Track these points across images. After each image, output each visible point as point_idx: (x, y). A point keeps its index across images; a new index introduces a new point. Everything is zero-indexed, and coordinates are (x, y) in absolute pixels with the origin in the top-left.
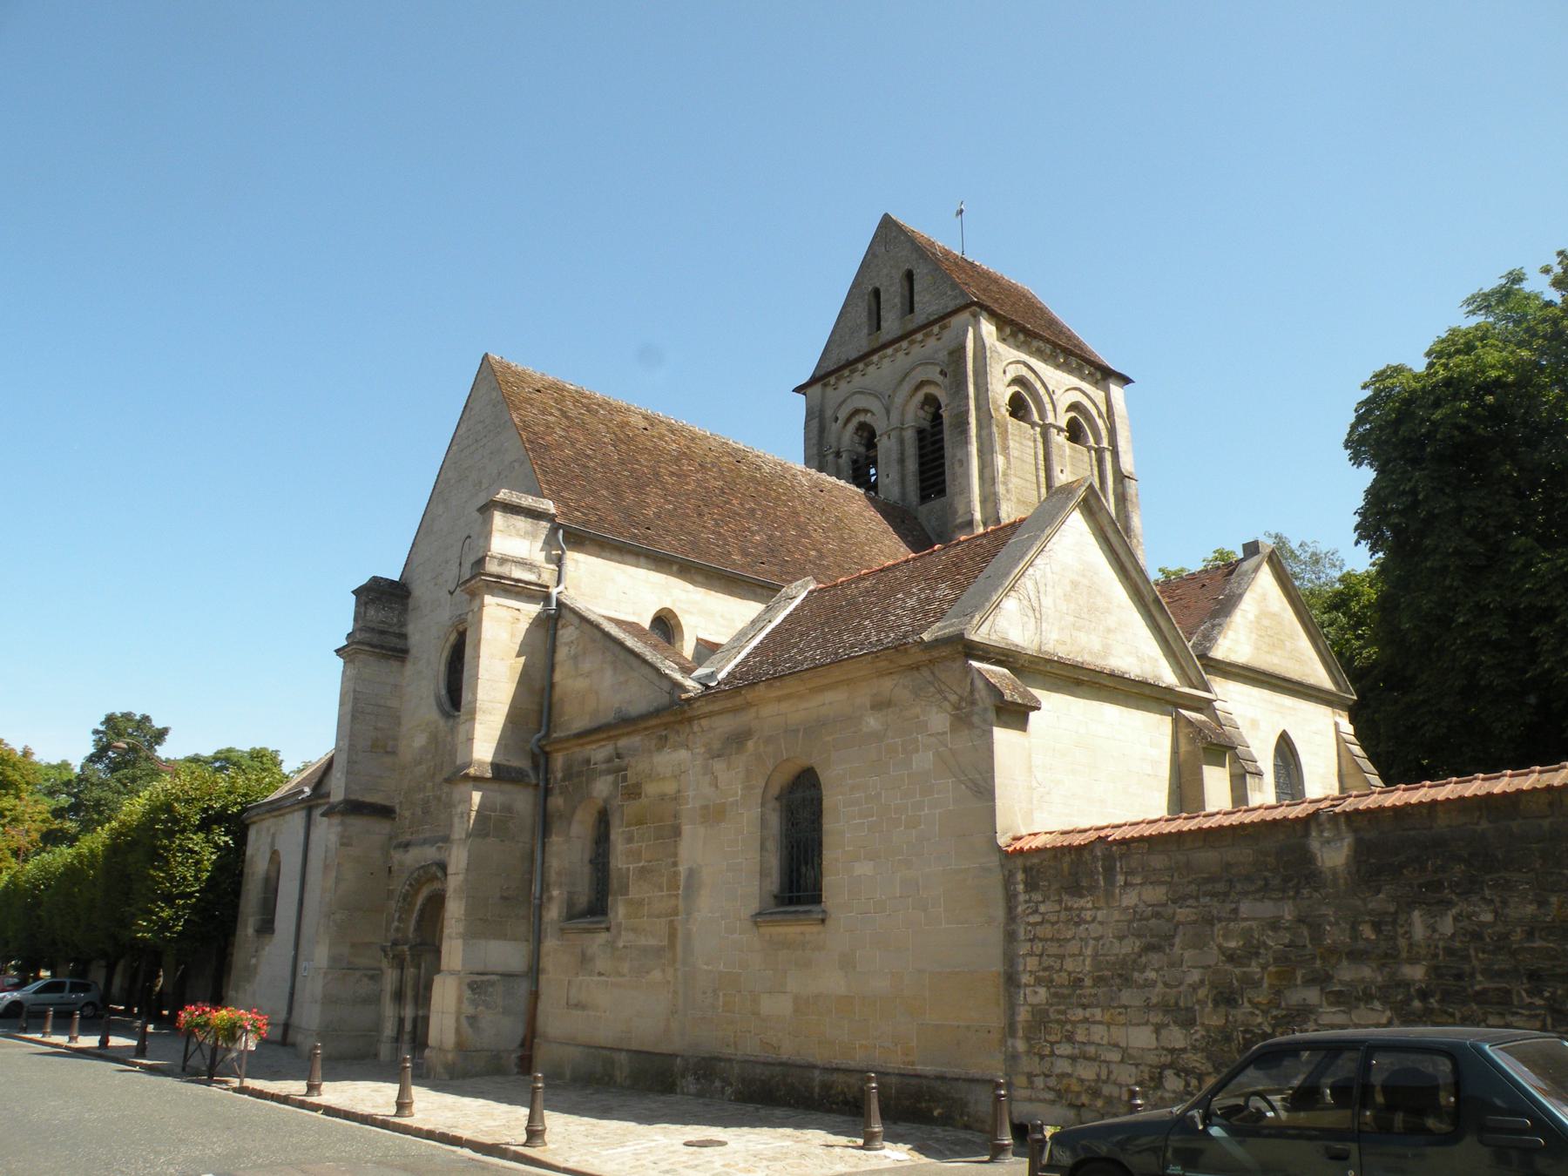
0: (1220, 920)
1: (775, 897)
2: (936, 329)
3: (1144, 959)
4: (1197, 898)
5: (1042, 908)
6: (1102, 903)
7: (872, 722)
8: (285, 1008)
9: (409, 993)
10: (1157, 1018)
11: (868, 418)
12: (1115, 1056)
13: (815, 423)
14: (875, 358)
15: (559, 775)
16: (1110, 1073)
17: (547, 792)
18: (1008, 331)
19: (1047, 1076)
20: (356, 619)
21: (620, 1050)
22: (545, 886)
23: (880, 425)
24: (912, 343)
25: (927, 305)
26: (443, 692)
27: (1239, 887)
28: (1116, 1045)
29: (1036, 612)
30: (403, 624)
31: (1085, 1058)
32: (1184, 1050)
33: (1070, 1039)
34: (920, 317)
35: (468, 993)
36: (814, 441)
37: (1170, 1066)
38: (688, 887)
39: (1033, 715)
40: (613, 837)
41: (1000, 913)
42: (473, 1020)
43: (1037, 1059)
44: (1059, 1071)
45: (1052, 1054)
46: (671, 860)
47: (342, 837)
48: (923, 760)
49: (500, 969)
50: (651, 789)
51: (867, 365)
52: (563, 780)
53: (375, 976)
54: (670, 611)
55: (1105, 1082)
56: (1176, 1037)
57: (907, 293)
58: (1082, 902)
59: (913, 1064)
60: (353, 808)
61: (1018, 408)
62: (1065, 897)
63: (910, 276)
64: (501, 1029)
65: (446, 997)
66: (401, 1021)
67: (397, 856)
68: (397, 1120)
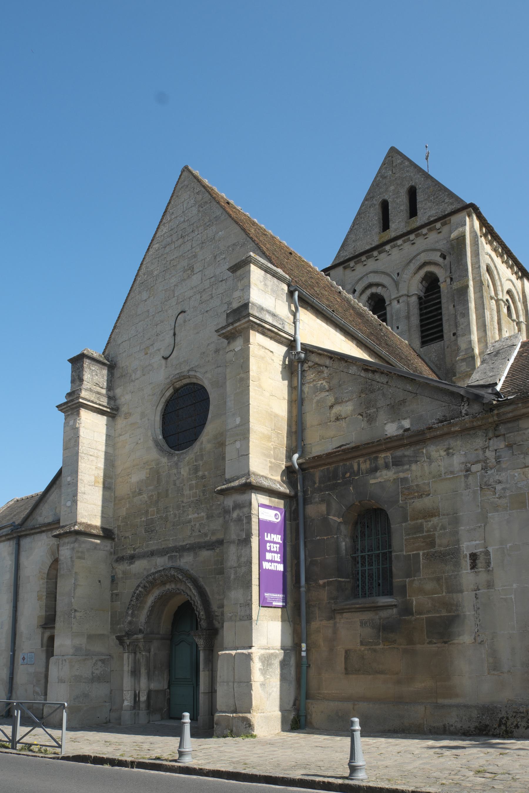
9: (143, 671)
11: (379, 290)
25: (427, 211)
26: (161, 437)
34: (422, 218)
63: (412, 193)
66: (136, 696)
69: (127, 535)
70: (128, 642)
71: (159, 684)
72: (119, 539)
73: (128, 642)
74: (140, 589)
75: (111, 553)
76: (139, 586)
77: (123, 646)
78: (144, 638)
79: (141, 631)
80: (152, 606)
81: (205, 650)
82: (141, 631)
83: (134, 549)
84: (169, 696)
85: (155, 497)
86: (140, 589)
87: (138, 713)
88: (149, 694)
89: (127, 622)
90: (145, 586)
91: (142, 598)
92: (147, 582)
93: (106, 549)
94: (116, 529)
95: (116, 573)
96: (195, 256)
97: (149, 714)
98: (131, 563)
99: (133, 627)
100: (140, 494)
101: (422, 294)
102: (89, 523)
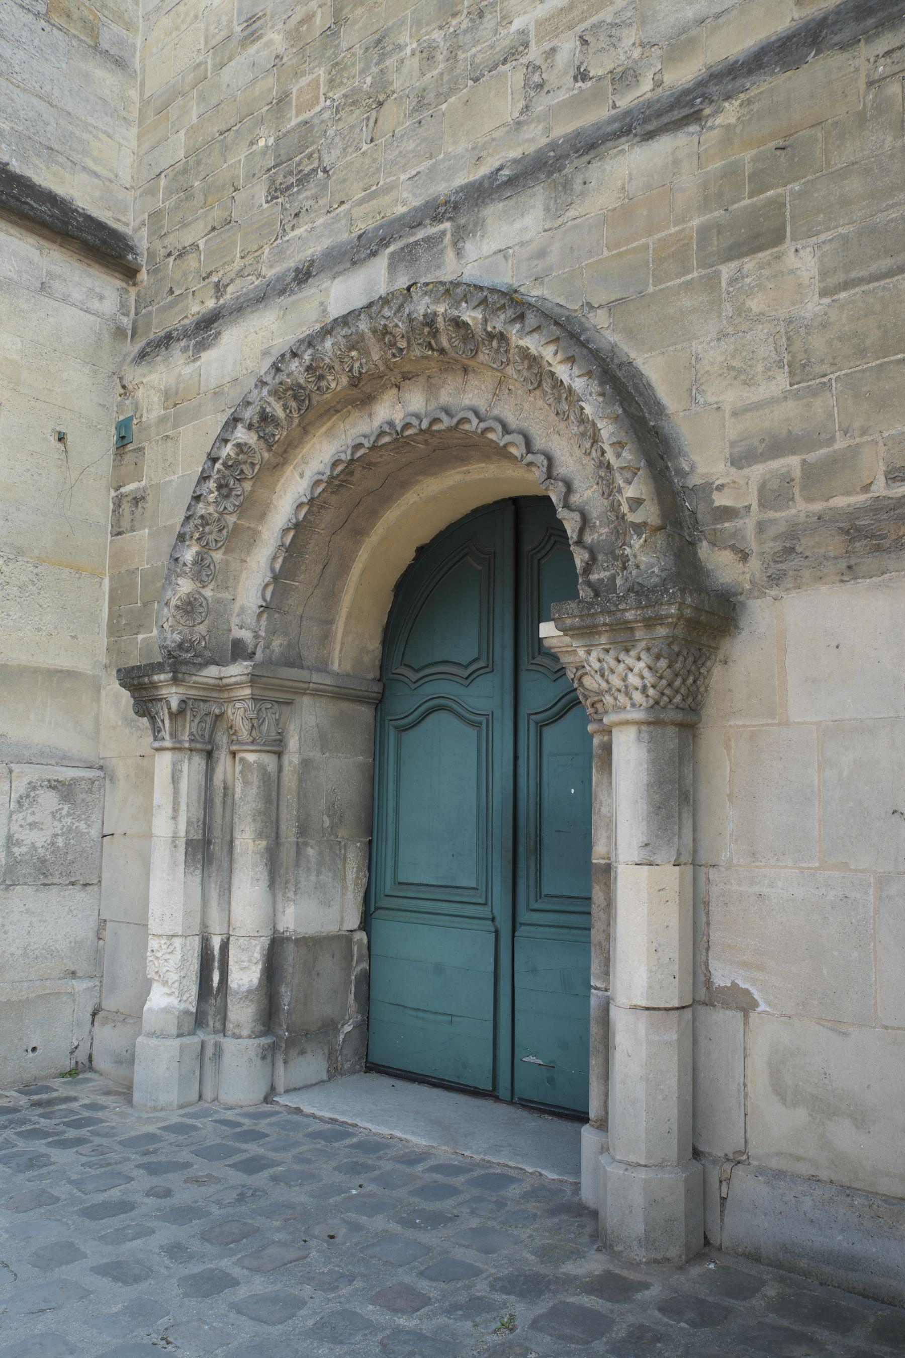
66: (210, 964)
69: (187, 238)
70: (173, 695)
71: (324, 908)
72: (152, 272)
73: (173, 695)
74: (241, 434)
75: (119, 333)
76: (235, 420)
77: (153, 720)
78: (254, 679)
79: (238, 651)
80: (297, 526)
81: (656, 723)
82: (238, 651)
83: (219, 289)
84: (365, 965)
86: (241, 434)
87: (218, 1052)
89: (173, 602)
90: (265, 418)
91: (248, 486)
92: (274, 393)
93: (95, 305)
94: (145, 232)
95: (137, 407)
97: (269, 1054)
98: (202, 346)
99: (202, 629)
100: (251, 36)
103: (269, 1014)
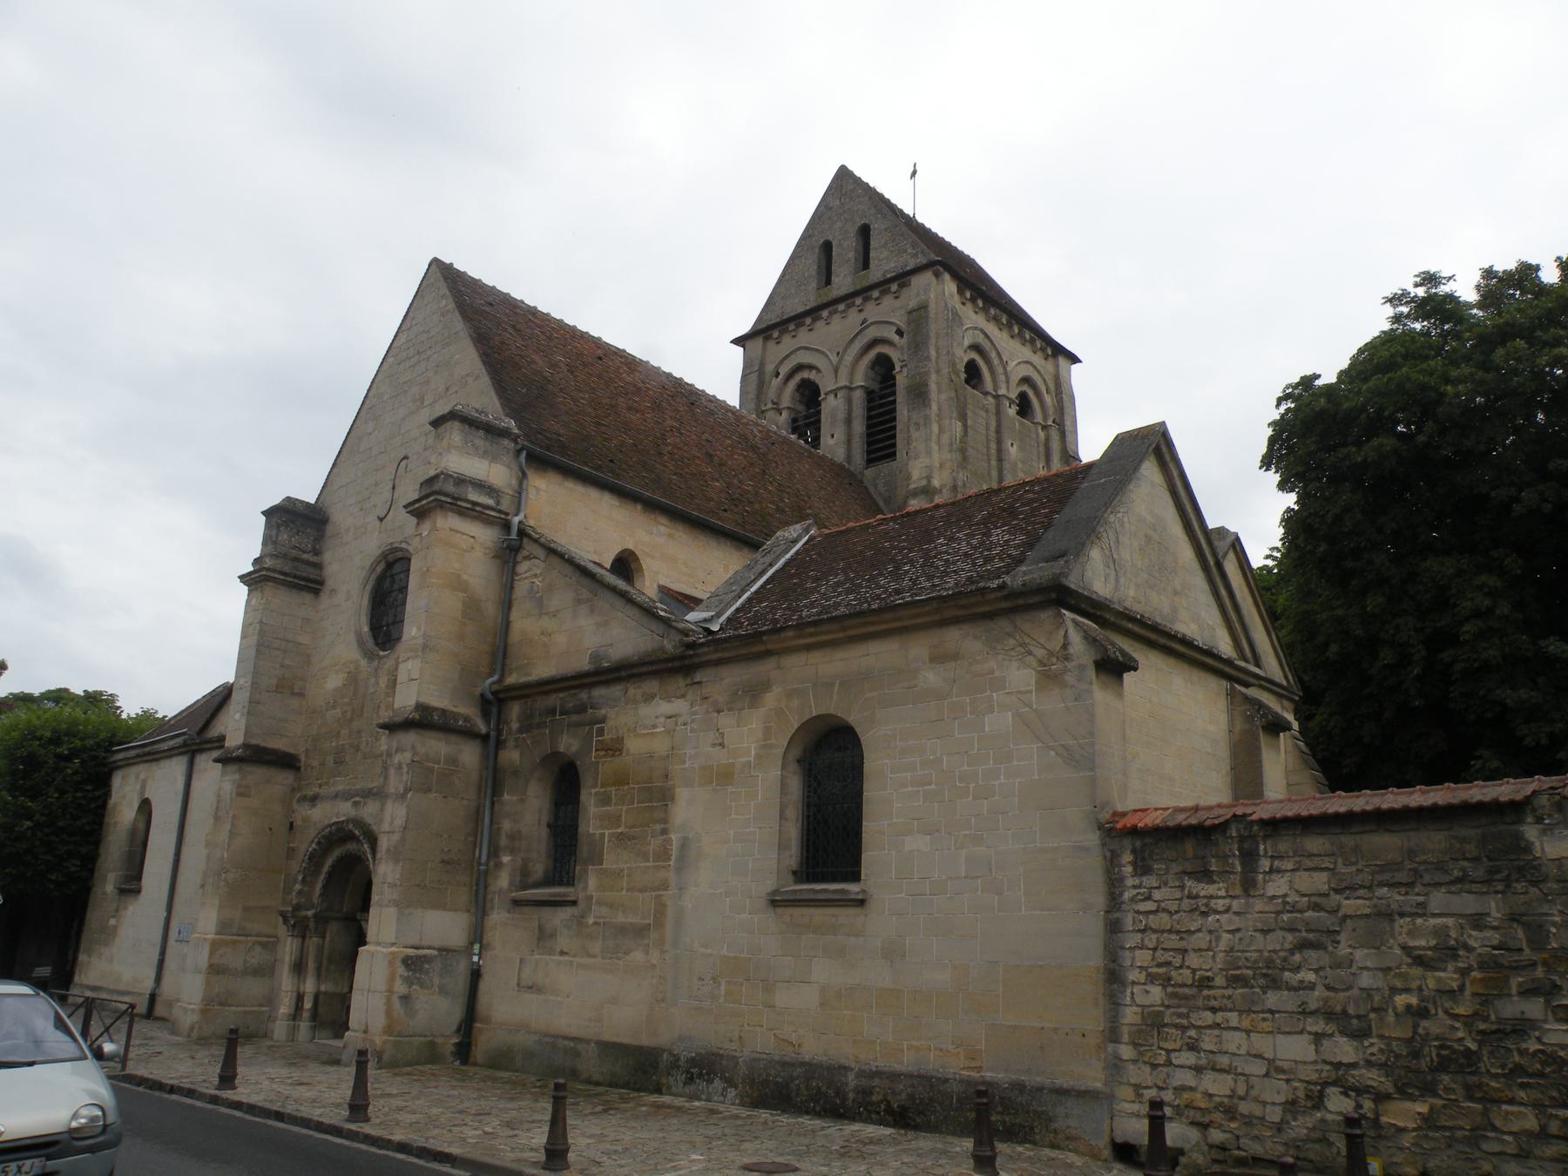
0: (1402, 915)
1: (794, 873)
2: (894, 287)
3: (1297, 957)
4: (1370, 888)
5: (1157, 895)
6: (1238, 891)
7: (931, 677)
8: (153, 975)
9: (311, 964)
10: (1318, 1026)
11: (812, 375)
12: (1258, 1068)
13: (754, 377)
14: (825, 314)
15: (515, 726)
16: (1250, 1087)
17: (499, 744)
18: (968, 295)
19: (1160, 1089)
20: (264, 544)
21: (588, 1041)
22: (494, 852)
23: (826, 383)
24: (866, 300)
25: (884, 263)
26: (366, 629)
27: (1427, 878)
28: (1260, 1056)
29: (1112, 561)
30: (317, 553)
31: (1213, 1069)
32: (1354, 1065)
33: (1193, 1047)
34: (875, 274)
35: (401, 970)
36: (752, 396)
37: (1334, 1083)
38: (682, 858)
39: (1128, 677)
40: (583, 797)
41: (1099, 900)
42: (405, 999)
43: (1147, 1069)
44: (1176, 1083)
45: (1169, 1063)
46: (658, 827)
47: (239, 786)
48: (1000, 721)
49: (438, 943)
50: (634, 746)
51: (814, 320)
52: (520, 731)
53: (270, 945)
54: (632, 553)
55: (1241, 1098)
56: (1344, 1049)
57: (824, 263)
58: (1211, 889)
59: (980, 1069)
60: (256, 756)
61: (972, 374)
62: (1189, 883)
63: (865, 232)
64: (438, 1011)
65: (374, 970)
66: (300, 998)
67: (304, 812)
68: (353, 1127)
85: (349, 715)
88: (317, 997)
96: (428, 382)
97: (314, 1028)
98: (314, 806)
100: (334, 707)
101: (875, 386)
102: (263, 744)
103: (314, 1015)
